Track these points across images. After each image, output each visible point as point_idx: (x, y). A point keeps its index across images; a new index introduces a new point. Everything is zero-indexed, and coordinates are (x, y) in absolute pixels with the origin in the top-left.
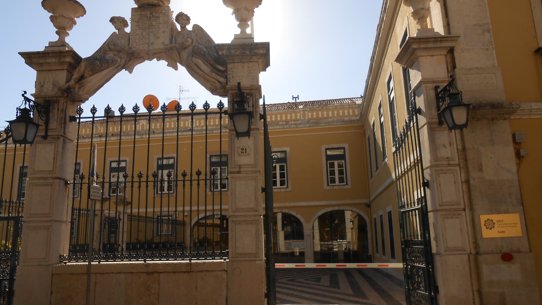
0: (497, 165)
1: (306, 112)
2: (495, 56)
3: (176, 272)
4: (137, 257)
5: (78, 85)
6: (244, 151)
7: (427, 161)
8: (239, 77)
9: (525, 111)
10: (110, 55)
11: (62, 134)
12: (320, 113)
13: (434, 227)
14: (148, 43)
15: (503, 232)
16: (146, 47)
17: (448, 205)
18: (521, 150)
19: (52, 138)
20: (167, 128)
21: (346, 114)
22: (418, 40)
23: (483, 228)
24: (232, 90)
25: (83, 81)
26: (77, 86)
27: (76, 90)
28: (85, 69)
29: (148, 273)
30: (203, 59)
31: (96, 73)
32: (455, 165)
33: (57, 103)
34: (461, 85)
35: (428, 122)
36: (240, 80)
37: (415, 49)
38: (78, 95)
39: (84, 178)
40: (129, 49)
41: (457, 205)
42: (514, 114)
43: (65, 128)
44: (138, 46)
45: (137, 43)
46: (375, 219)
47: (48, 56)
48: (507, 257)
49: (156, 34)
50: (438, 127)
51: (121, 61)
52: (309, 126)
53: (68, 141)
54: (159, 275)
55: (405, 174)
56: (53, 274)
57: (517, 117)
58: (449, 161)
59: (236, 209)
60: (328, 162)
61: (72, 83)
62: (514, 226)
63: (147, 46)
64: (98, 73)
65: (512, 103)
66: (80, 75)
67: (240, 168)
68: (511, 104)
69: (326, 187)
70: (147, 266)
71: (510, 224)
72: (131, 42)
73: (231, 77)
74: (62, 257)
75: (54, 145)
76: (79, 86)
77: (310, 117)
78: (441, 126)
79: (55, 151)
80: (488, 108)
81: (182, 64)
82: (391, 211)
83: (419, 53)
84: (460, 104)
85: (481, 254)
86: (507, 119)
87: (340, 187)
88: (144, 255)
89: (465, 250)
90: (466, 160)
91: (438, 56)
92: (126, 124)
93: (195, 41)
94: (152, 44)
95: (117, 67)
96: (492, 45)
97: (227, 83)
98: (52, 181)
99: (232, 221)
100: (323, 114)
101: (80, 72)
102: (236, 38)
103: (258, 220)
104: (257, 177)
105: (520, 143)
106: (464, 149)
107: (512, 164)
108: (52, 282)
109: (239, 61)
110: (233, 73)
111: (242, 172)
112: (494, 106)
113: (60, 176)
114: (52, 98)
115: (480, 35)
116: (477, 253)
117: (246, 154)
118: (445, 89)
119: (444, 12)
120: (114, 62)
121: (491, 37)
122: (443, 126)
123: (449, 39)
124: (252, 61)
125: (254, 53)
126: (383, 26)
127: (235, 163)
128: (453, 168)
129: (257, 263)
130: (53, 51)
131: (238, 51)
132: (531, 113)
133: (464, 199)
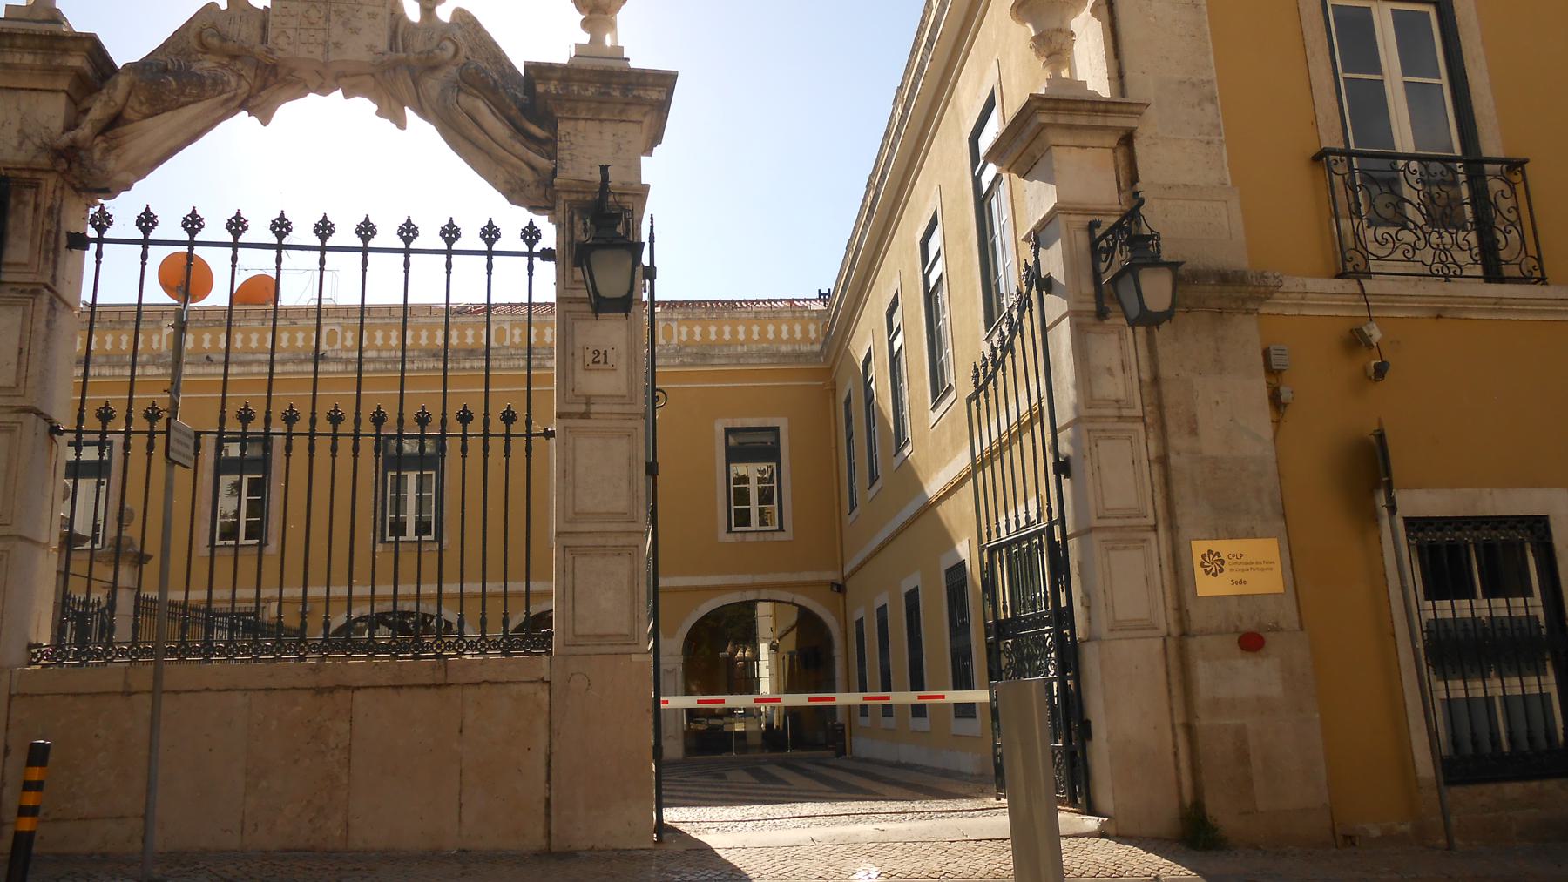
0: (1231, 420)
1: (674, 325)
2: (1226, 161)
3: (401, 687)
4: (278, 650)
5: (104, 141)
6: (600, 358)
7: (1064, 414)
8: (590, 159)
9: (1291, 296)
10: (207, 64)
11: (47, 280)
12: (713, 329)
13: (1081, 574)
14: (325, 44)
15: (1242, 582)
16: (318, 53)
17: (1117, 518)
18: (1282, 389)
19: (13, 289)
20: (251, 348)
21: (785, 336)
22: (1051, 105)
23: (1199, 571)
24: (569, 191)
25: (118, 129)
26: (100, 144)
27: (97, 155)
28: (129, 94)
29: (318, 691)
30: (491, 102)
31: (164, 111)
32: (1134, 419)
33: (32, 187)
34: (1154, 217)
35: (1072, 311)
36: (591, 167)
37: (1043, 126)
38: (102, 171)
39: (112, 418)
40: (267, 52)
41: (1138, 517)
42: (1268, 301)
43: (55, 263)
44: (288, 45)
45: (292, 39)
46: (860, 623)
47: (12, 46)
48: (1251, 642)
49: (349, 20)
50: (1094, 325)
51: (239, 86)
52: (683, 364)
53: (62, 305)
54: (350, 694)
55: (1031, 423)
56: (14, 695)
57: (1274, 311)
58: (1120, 408)
59: (575, 513)
60: (389, 474)
61: (85, 131)
62: (1267, 569)
63: (320, 50)
64: (169, 110)
65: (1265, 274)
66: (112, 111)
67: (588, 404)
68: (1263, 276)
69: (723, 536)
70: (314, 670)
71: (1257, 563)
72: (272, 34)
73: (569, 157)
74: (35, 651)
75: (20, 312)
76: (105, 145)
77: (684, 338)
78: (1102, 320)
79: (22, 330)
80: (1213, 282)
81: (422, 112)
82: (917, 587)
83: (1052, 137)
84: (1156, 262)
85: (1194, 636)
86: (1252, 314)
87: (761, 537)
88: (298, 643)
89: (1156, 628)
90: (1160, 407)
91: (1096, 149)
92: (114, 329)
93: (464, 51)
94: (337, 45)
95: (227, 101)
96: (1220, 135)
97: (554, 172)
98: (13, 417)
99: (565, 547)
100: (720, 333)
101: (112, 104)
102: (581, 54)
103: (637, 546)
104: (634, 431)
105: (1280, 371)
106: (1156, 380)
107: (1261, 420)
108: (8, 718)
109: (589, 117)
110: (573, 147)
111: (592, 416)
112: (1226, 278)
113: (37, 406)
114: (16, 173)
115: (1193, 107)
116: (1184, 634)
117: (606, 366)
118: (1116, 229)
119: (1110, 44)
120: (218, 85)
121: (1218, 116)
122: (1106, 322)
123: (1124, 108)
124: (624, 118)
125: (634, 96)
126: (920, 86)
127: (573, 390)
128: (1130, 426)
129: (633, 660)
130: (31, 32)
131: (590, 89)
132: (1303, 302)
133: (1154, 504)
